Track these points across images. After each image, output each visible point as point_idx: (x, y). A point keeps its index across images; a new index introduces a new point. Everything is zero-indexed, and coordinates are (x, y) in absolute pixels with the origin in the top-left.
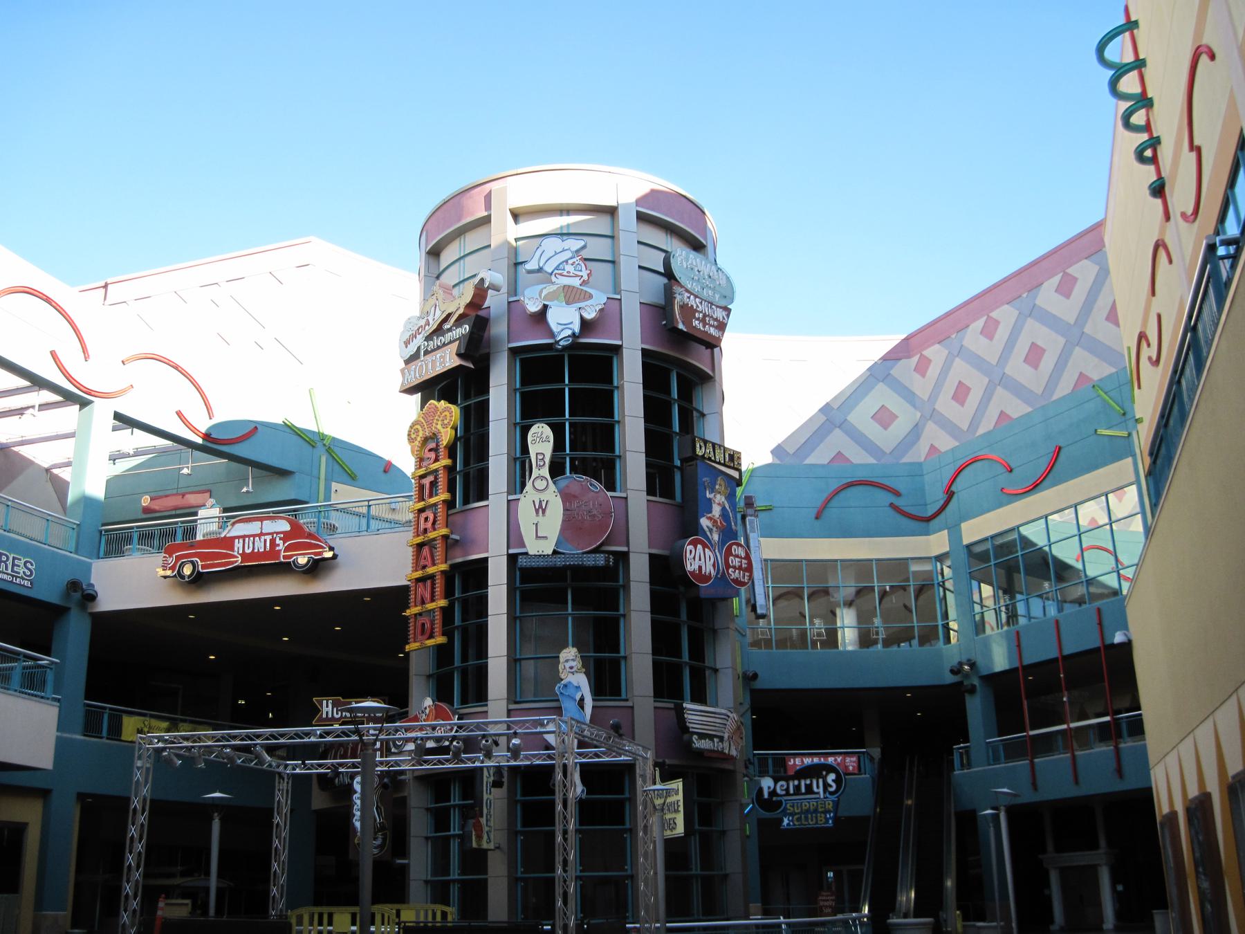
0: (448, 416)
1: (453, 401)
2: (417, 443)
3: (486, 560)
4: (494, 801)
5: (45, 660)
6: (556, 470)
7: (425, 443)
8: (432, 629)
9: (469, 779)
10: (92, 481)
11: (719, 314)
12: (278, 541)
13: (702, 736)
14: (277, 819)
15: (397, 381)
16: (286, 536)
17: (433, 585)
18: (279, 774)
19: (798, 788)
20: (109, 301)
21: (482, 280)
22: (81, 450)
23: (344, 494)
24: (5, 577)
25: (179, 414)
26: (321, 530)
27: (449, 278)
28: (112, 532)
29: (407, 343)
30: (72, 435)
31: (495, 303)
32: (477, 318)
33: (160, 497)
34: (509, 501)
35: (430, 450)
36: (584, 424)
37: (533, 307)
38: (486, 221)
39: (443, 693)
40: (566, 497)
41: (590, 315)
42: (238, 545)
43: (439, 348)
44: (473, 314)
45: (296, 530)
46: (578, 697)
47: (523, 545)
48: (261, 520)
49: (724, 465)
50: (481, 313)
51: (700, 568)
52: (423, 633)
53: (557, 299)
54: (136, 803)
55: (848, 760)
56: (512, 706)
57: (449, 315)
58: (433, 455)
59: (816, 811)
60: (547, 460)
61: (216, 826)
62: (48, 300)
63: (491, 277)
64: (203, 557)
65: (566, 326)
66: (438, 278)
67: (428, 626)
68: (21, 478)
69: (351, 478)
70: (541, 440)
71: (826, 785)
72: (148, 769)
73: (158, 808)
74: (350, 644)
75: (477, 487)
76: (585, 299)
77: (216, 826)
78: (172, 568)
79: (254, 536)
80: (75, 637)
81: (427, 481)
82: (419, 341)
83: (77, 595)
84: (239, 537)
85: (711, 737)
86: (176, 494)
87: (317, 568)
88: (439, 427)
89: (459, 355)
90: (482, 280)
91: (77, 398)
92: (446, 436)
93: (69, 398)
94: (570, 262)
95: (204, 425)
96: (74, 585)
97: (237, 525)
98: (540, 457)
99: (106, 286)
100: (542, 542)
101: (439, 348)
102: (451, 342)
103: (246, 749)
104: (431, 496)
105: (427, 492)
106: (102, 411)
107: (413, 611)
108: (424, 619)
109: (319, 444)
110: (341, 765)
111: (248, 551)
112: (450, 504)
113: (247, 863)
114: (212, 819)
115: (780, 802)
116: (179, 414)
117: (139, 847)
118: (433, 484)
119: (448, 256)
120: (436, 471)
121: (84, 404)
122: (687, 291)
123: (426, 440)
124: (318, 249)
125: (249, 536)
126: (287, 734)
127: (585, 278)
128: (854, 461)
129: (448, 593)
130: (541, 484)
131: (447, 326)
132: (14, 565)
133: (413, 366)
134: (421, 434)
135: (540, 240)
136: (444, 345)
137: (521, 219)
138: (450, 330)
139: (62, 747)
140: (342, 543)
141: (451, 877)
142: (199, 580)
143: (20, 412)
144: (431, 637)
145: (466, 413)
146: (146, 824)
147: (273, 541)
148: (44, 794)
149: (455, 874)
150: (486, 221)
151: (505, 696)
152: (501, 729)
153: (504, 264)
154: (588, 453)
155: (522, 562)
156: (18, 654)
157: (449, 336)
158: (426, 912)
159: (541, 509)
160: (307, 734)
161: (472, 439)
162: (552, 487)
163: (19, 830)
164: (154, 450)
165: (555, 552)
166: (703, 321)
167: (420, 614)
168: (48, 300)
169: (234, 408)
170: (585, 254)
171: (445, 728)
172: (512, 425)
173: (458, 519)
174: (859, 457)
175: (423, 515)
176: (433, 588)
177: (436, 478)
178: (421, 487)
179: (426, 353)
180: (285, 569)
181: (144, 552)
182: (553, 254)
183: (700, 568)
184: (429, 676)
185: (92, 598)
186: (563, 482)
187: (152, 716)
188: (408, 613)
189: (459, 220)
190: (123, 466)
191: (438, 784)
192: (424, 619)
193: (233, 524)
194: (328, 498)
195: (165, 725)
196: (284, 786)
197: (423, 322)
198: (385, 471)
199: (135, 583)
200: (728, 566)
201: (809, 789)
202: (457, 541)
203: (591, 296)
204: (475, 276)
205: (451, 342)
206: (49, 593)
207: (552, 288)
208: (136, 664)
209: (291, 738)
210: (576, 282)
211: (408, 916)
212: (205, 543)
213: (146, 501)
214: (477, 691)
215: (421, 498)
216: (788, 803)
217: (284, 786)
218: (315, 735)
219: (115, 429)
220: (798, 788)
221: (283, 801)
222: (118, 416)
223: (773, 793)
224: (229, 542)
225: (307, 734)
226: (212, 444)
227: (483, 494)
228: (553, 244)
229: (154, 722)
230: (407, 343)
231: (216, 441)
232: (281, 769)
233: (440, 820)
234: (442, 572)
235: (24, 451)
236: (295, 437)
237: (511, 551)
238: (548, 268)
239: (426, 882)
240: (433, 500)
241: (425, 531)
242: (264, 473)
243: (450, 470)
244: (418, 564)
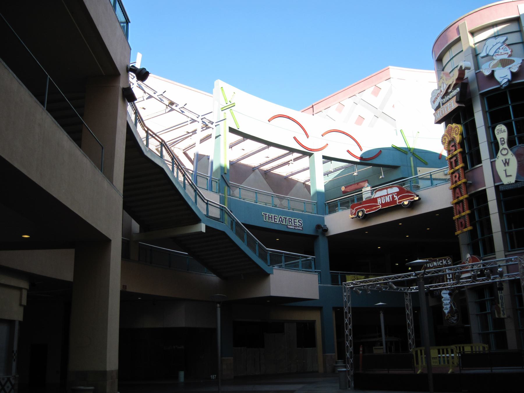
0: (458, 128)
1: (458, 122)
2: (446, 144)
3: (485, 190)
4: (504, 295)
5: (310, 257)
6: (511, 143)
7: (450, 143)
8: (465, 224)
9: (492, 288)
10: (320, 185)
12: (395, 196)
14: (407, 312)
15: (433, 119)
16: (398, 194)
17: (463, 204)
18: (406, 293)
20: (315, 112)
21: (461, 67)
22: (313, 174)
23: (423, 171)
24: (292, 227)
25: (348, 151)
26: (412, 189)
27: (448, 69)
28: (330, 202)
29: (434, 102)
30: (308, 169)
31: (469, 74)
32: (462, 82)
33: (349, 186)
34: (491, 162)
35: (452, 146)
37: (487, 73)
38: (459, 40)
39: (475, 252)
40: (518, 155)
41: (515, 70)
42: (379, 201)
43: (448, 101)
44: (460, 82)
45: (402, 191)
47: (501, 181)
48: (387, 188)
50: (464, 81)
52: (462, 226)
53: (498, 66)
54: (346, 310)
56: (507, 253)
57: (450, 86)
58: (454, 148)
60: (506, 140)
61: (382, 316)
62: (289, 118)
63: (464, 64)
64: (366, 207)
65: (504, 77)
66: (443, 70)
67: (463, 222)
68: (294, 188)
69: (425, 164)
70: (502, 132)
72: (349, 296)
73: (355, 311)
74: (432, 235)
75: (477, 159)
77: (382, 316)
78: (355, 214)
79: (385, 196)
80: (322, 247)
81: (453, 160)
82: (439, 100)
83: (320, 230)
84: (379, 197)
86: (354, 184)
87: (413, 205)
88: (454, 135)
90: (461, 67)
91: (307, 153)
92: (458, 138)
93: (305, 154)
94: (501, 48)
95: (359, 154)
96: (318, 227)
97: (377, 193)
98: (502, 140)
99: (313, 107)
100: (509, 178)
101: (448, 101)
102: (453, 97)
103: (385, 284)
104: (456, 166)
105: (454, 164)
106: (318, 156)
107: (456, 217)
108: (462, 220)
109: (409, 153)
110: (431, 287)
111: (383, 202)
112: (465, 168)
113: (397, 329)
114: (379, 314)
116: (348, 151)
117: (350, 327)
118: (456, 162)
119: (445, 60)
120: (456, 155)
121: (310, 155)
123: (450, 142)
124: (394, 71)
125: (383, 196)
126: (401, 276)
129: (470, 207)
130: (504, 152)
131: (449, 91)
132: (294, 222)
133: (438, 111)
135: (484, 42)
136: (450, 99)
137: (475, 34)
138: (451, 92)
139: (322, 290)
140: (423, 193)
141: (490, 331)
142: (366, 217)
143: (287, 163)
144: (465, 227)
145: (466, 127)
146: (351, 317)
147: (393, 196)
148: (320, 309)
149: (491, 330)
150: (459, 40)
151: (503, 249)
152: (504, 263)
153: (471, 57)
155: (501, 188)
156: (299, 256)
157: (451, 95)
158: (460, 348)
159: (506, 163)
160: (410, 276)
161: (470, 138)
162: (510, 152)
163: (313, 323)
164: (342, 168)
165: (516, 181)
167: (460, 218)
168: (289, 118)
169: (371, 144)
170: (508, 42)
171: (479, 265)
172: (487, 128)
173: (469, 174)
175: (454, 175)
176: (463, 206)
177: (457, 158)
178: (451, 163)
179: (443, 104)
180: (400, 207)
181: (343, 209)
182: (491, 48)
184: (468, 244)
185: (326, 230)
186: (515, 149)
187: (358, 274)
188: (454, 218)
189: (447, 43)
190: (331, 177)
191: (479, 290)
192: (462, 220)
193: (376, 192)
194: (416, 174)
195: (363, 277)
196: (408, 298)
197: (439, 91)
198: (440, 159)
199: (341, 222)
202: (471, 184)
203: (513, 61)
204: (457, 67)
205: (453, 97)
206: (310, 231)
207: (494, 62)
208: (345, 254)
209: (403, 278)
210: (505, 57)
211: (468, 349)
212: (366, 202)
213: (343, 188)
214: (490, 249)
215: (452, 168)
217: (408, 298)
218: (413, 275)
219: (324, 163)
221: (409, 304)
222: (324, 157)
224: (375, 200)
225: (410, 276)
226: (364, 161)
227: (480, 162)
228: (493, 41)
229: (359, 277)
230: (434, 102)
231: (365, 160)
232: (406, 291)
233: (482, 306)
234: (466, 198)
235: (294, 177)
236: (398, 152)
237: (496, 184)
238: (491, 54)
239: (479, 334)
240: (457, 168)
241: (456, 182)
242: (388, 169)
243: (463, 153)
244: (455, 196)
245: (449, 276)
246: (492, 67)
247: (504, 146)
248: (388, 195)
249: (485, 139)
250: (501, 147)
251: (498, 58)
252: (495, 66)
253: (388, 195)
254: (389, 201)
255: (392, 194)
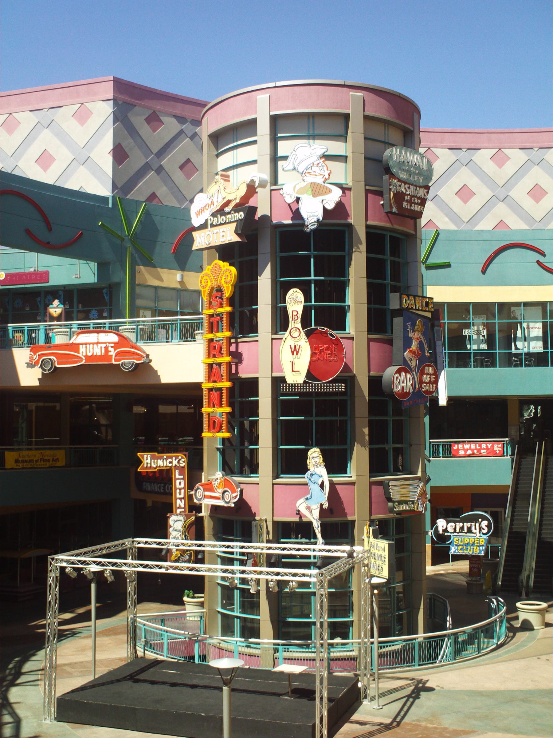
6: (305, 321)
11: (421, 193)
12: (110, 349)
13: (400, 503)
16: (116, 345)
19: (462, 528)
36: (323, 256)
39: (227, 468)
42: (82, 349)
46: (320, 483)
49: (422, 310)
51: (403, 388)
55: (496, 446)
57: (228, 202)
59: (473, 544)
60: (300, 315)
70: (295, 301)
71: (481, 529)
76: (326, 193)
79: (93, 344)
84: (82, 344)
85: (406, 502)
89: (236, 232)
115: (450, 536)
122: (400, 180)
125: (90, 344)
127: (327, 177)
128: (513, 228)
131: (227, 209)
134: (209, 284)
138: (229, 213)
147: (106, 348)
154: (325, 318)
159: (295, 351)
165: (305, 382)
166: (411, 202)
174: (516, 224)
179: (212, 226)
183: (403, 388)
200: (421, 382)
201: (469, 530)
205: (230, 222)
210: (320, 181)
216: (455, 538)
220: (462, 528)
223: (445, 530)
245: (180, 494)
246: (297, 193)
247: (295, 324)
248: (97, 343)
249: (206, 152)
250: (291, 325)
251: (310, 179)
252: (303, 190)
253: (97, 343)
254: (99, 354)
255: (105, 343)
